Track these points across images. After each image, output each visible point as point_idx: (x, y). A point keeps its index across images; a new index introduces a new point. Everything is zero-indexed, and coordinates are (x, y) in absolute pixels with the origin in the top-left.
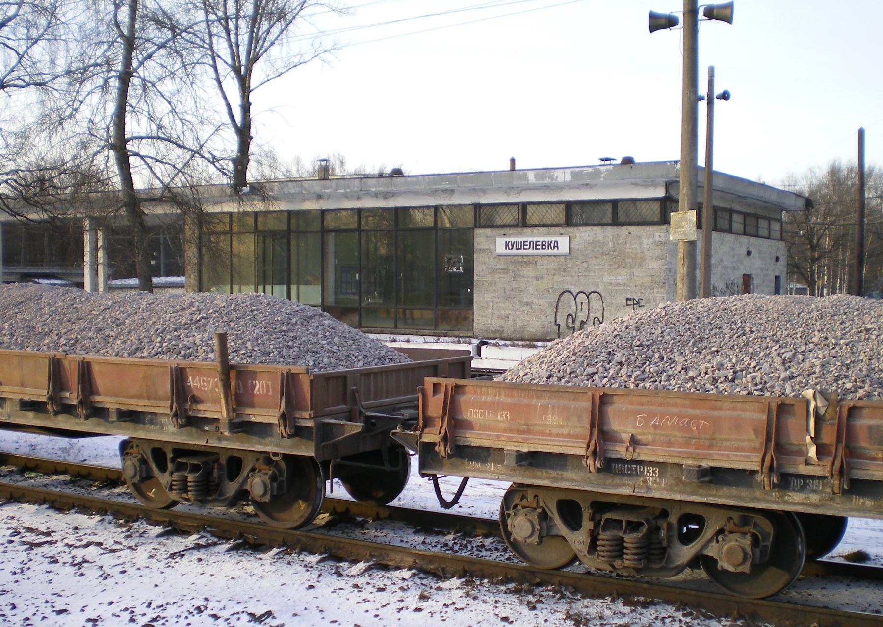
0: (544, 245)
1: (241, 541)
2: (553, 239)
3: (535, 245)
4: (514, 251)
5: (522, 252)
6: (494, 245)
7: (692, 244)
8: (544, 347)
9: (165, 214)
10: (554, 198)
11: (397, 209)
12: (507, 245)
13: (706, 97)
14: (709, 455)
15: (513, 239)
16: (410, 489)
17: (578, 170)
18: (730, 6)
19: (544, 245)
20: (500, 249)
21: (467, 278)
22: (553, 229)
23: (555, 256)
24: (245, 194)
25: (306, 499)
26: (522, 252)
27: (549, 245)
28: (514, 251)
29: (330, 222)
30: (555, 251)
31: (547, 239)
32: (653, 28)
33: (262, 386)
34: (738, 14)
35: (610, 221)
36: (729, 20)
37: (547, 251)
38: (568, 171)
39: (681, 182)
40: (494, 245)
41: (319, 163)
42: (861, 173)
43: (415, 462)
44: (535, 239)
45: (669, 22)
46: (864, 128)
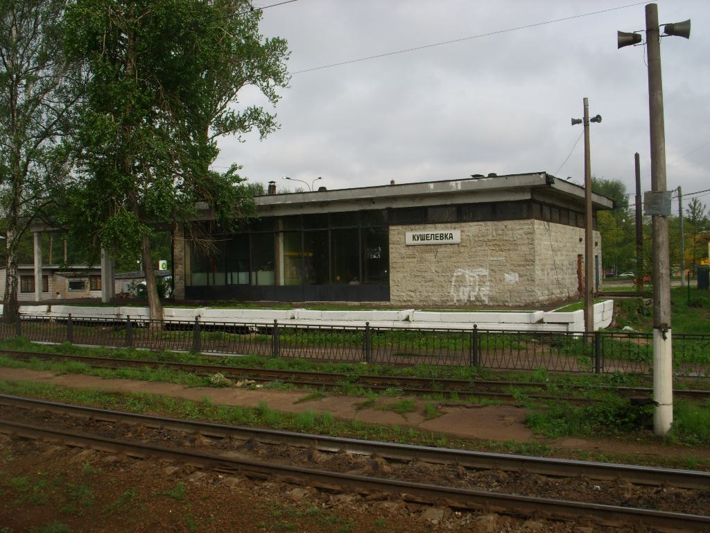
0: (597, 261)
1: (58, 229)
2: (449, 232)
3: (435, 237)
4: (420, 242)
5: (425, 242)
6: (403, 237)
7: (580, 256)
8: (495, 405)
9: (248, 270)
10: (449, 202)
11: (676, 393)
12: (414, 237)
13: (583, 121)
14: (365, 304)
15: (418, 233)
16: (597, 324)
17: (356, 208)
18: (688, 23)
19: (442, 237)
20: (409, 240)
21: (384, 262)
22: (589, 271)
23: (426, 245)
24: (237, 387)
25: (462, 514)
26: (425, 242)
27: (446, 236)
28: (420, 242)
29: (616, 362)
30: (450, 241)
31: (444, 232)
32: (621, 45)
33: (627, 524)
34: (615, 40)
35: (429, 209)
36: (620, 34)
37: (444, 241)
38: (459, 182)
39: (103, 274)
40: (403, 237)
41: (268, 184)
42: (657, 197)
43: (453, 462)
44: (435, 233)
45: (594, 120)
46: (639, 153)
